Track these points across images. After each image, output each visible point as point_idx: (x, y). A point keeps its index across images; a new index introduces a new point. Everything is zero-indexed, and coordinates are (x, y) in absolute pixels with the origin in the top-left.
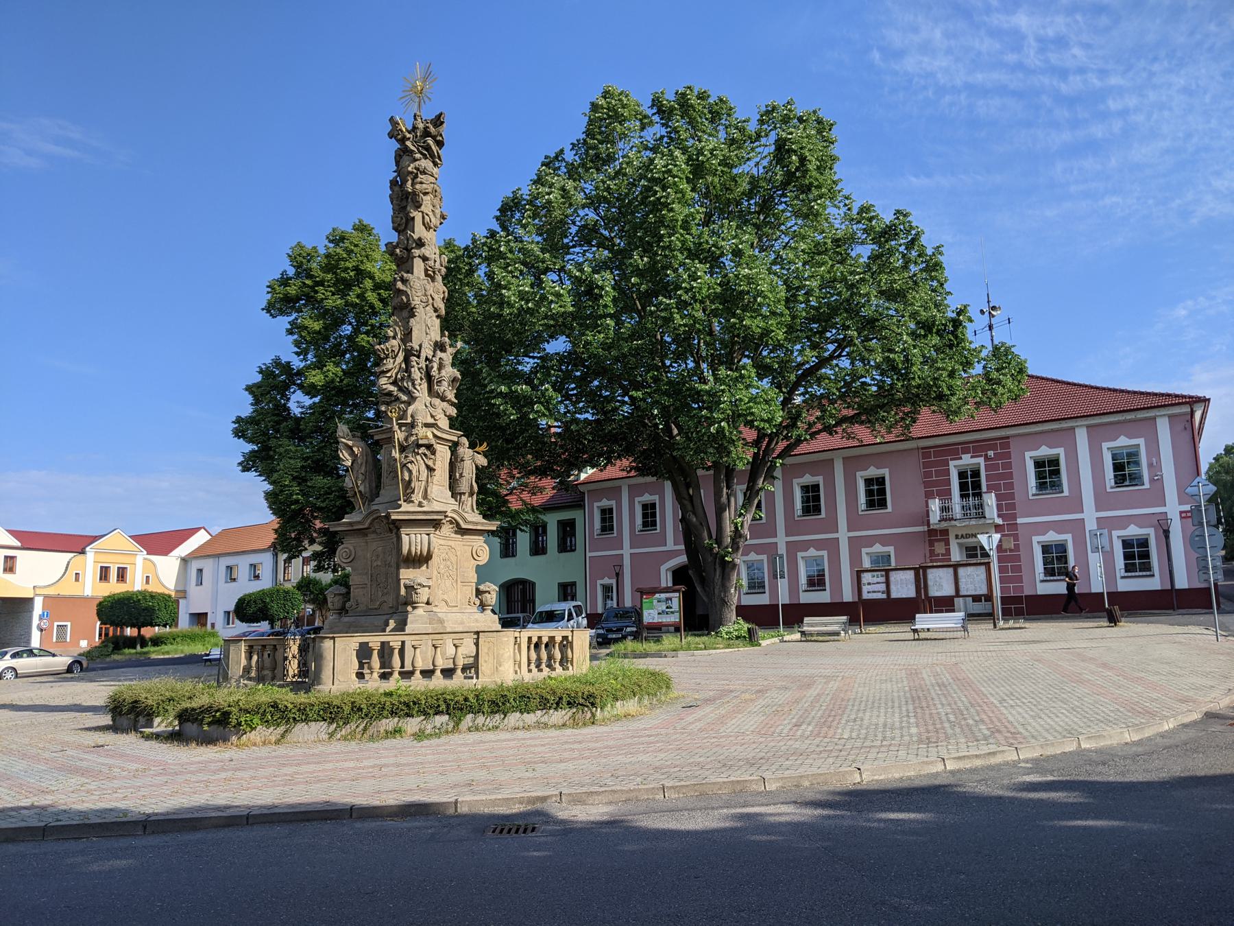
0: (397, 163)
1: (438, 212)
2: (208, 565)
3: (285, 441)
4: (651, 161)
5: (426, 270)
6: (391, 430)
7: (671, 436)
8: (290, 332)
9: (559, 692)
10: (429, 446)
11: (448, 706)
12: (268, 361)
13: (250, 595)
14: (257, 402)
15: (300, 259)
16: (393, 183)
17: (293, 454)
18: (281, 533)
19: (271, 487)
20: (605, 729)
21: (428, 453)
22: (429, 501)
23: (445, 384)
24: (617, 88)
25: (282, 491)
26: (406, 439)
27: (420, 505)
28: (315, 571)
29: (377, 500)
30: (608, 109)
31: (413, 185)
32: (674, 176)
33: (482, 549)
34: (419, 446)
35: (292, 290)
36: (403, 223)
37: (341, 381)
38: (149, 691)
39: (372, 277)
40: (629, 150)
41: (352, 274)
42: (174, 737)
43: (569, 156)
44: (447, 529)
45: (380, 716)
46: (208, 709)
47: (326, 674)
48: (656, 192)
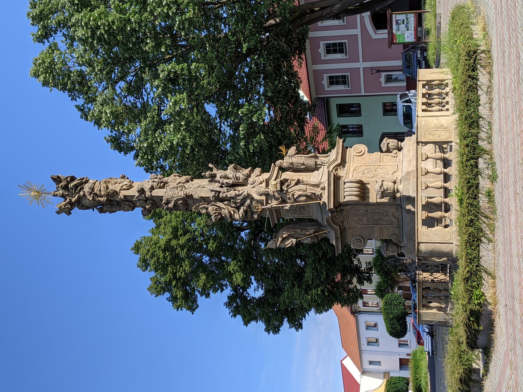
0: (88, 208)
1: (120, 180)
2: (367, 358)
3: (282, 298)
4: (80, 39)
5: (160, 187)
6: (270, 210)
7: (277, 25)
8: (208, 296)
9: (464, 78)
10: (282, 183)
11: (472, 158)
12: (227, 310)
13: (388, 328)
14: (255, 319)
15: (158, 289)
16: (101, 211)
17: (291, 294)
18: (344, 302)
19: (313, 309)
20: (494, 43)
21: (286, 184)
22: (320, 183)
23: (238, 174)
24: (32, 68)
25: (315, 301)
26: (277, 199)
27: (323, 189)
28: (371, 282)
29: (320, 220)
30: (46, 73)
31: (102, 197)
32: (89, 20)
33: (358, 148)
34: (282, 190)
35: (180, 294)
36: (128, 203)
37: (240, 261)
38: (453, 372)
39: (170, 240)
40: (73, 58)
41: (167, 254)
42: (487, 352)
43: (80, 101)
44: (341, 172)
45: (477, 207)
46: (468, 326)
47: (445, 248)
48: (101, 34)
